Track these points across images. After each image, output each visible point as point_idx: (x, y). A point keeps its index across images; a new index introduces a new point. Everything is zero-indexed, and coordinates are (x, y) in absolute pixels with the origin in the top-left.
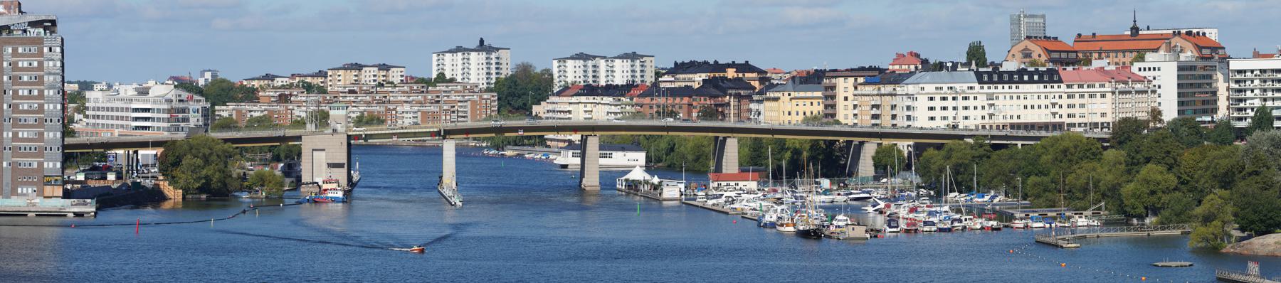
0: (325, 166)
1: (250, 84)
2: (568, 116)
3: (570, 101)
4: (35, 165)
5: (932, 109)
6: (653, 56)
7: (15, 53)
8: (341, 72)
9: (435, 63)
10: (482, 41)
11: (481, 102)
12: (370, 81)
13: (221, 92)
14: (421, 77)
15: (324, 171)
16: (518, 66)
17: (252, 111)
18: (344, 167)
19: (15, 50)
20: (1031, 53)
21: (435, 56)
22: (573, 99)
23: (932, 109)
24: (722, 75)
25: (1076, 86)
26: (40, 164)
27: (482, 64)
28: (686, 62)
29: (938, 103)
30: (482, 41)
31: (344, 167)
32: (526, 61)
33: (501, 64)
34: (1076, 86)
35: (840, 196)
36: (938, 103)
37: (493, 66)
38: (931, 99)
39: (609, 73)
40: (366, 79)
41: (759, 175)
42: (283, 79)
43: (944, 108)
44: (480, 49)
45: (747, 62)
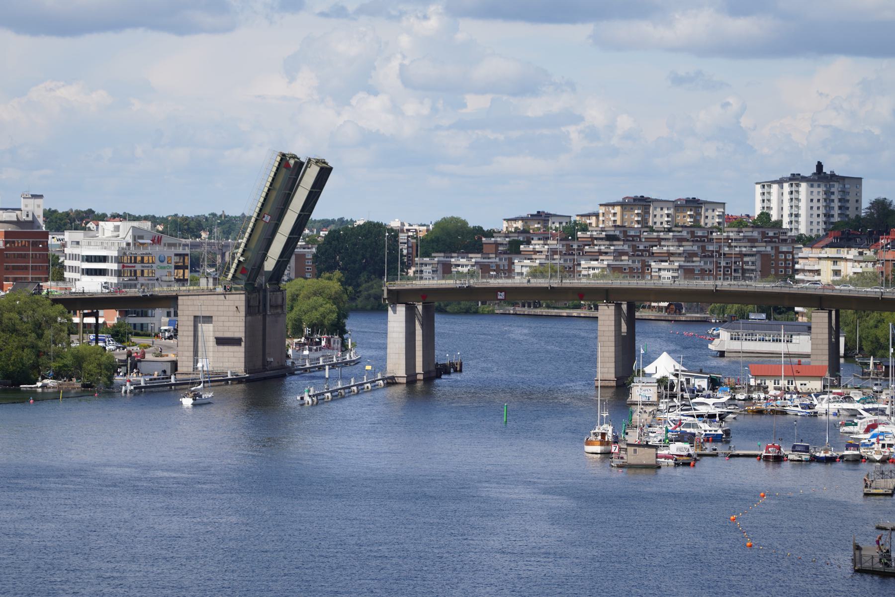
0: (212, 342)
1: (512, 226)
2: (816, 278)
3: (821, 255)
8: (618, 209)
9: (759, 198)
10: (820, 166)
11: (777, 255)
12: (662, 223)
14: (450, 216)
15: (211, 349)
17: (459, 265)
18: (240, 345)
20: (225, 215)
21: (758, 187)
22: (823, 252)
27: (819, 200)
28: (157, 216)
30: (820, 166)
31: (240, 345)
32: (114, 212)
33: (848, 201)
37: (836, 204)
39: (793, 218)
40: (655, 220)
41: (825, 366)
42: (561, 220)
44: (816, 178)
45: (243, 214)
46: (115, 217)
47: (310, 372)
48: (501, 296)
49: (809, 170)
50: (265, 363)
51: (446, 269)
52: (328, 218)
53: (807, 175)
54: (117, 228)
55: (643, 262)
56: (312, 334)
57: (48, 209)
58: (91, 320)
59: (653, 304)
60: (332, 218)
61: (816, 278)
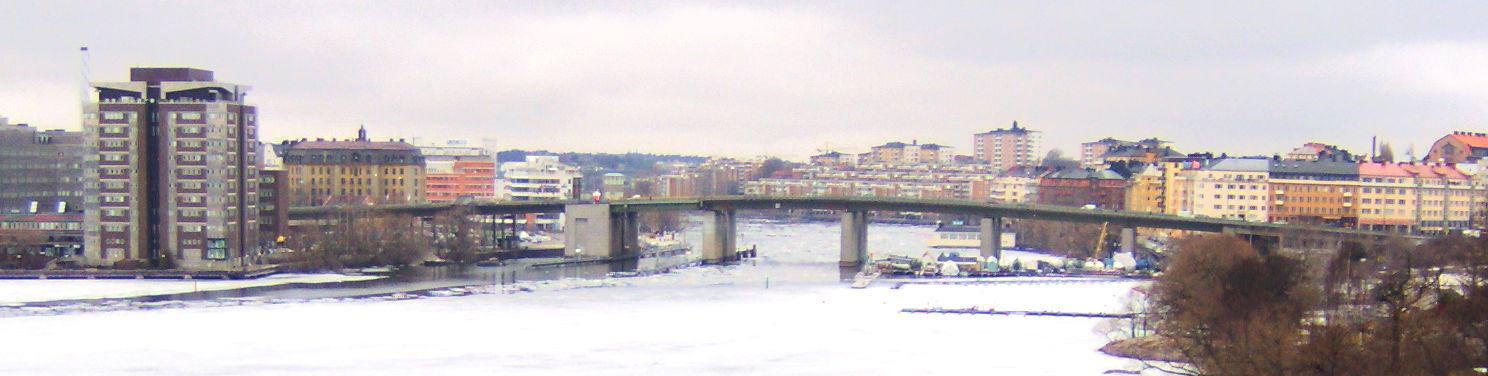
4: (199, 229)
5: (1218, 197)
6: (1374, 138)
7: (179, 120)
10: (1015, 124)
13: (1334, 163)
16: (1051, 152)
19: (179, 116)
23: (1218, 197)
24: (638, 180)
25: (1374, 181)
26: (204, 228)
29: (1224, 191)
30: (1015, 124)
34: (1374, 181)
35: (340, 184)
36: (1224, 191)
38: (1219, 186)
43: (1254, 198)
46: (535, 154)
47: (271, 269)
48: (778, 206)
49: (1008, 127)
50: (624, 251)
51: (768, 187)
52: (32, 124)
53: (1008, 129)
54: (537, 161)
55: (896, 185)
56: (461, 235)
57: (396, 140)
58: (508, 221)
59: (903, 213)
60: (34, 126)
61: (1003, 197)
